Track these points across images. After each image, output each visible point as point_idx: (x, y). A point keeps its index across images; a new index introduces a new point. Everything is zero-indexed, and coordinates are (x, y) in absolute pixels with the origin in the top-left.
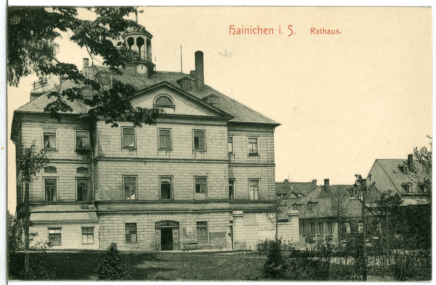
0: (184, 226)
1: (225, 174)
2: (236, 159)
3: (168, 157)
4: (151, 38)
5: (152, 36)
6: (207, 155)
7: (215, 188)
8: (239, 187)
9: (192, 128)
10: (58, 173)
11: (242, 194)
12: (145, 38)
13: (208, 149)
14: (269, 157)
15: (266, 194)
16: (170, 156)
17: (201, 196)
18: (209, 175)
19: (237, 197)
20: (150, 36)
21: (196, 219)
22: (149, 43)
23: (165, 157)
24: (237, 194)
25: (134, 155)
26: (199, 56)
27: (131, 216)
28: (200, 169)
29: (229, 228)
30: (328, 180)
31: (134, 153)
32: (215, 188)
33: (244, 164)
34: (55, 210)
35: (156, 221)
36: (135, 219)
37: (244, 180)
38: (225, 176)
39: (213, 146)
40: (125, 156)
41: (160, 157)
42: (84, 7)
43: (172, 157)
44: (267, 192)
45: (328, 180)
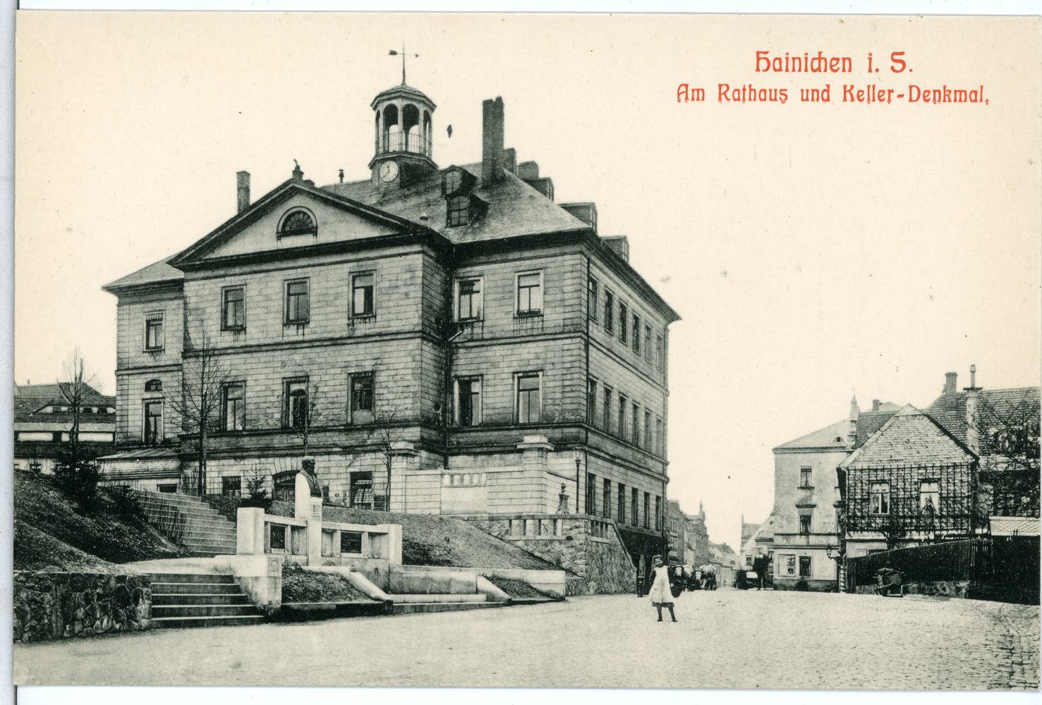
0: (326, 483)
1: (414, 363)
2: (485, 330)
3: (301, 338)
4: (433, 110)
5: (435, 106)
6: (377, 324)
7: (391, 396)
8: (490, 395)
9: (282, 278)
10: (165, 390)
11: (497, 411)
12: (422, 109)
13: (379, 311)
14: (567, 316)
15: (557, 407)
16: (304, 335)
17: (362, 416)
18: (382, 367)
19: (484, 417)
20: (432, 107)
21: (349, 466)
22: (428, 119)
23: (296, 338)
24: (485, 412)
25: (242, 340)
26: (295, 160)
27: (232, 462)
28: (360, 357)
29: (776, 576)
30: (955, 375)
31: (242, 337)
32: (391, 396)
33: (504, 338)
34: (41, 429)
35: (274, 473)
36: (239, 468)
37: (504, 376)
38: (412, 368)
39: (391, 304)
40: (226, 345)
41: (286, 339)
42: (404, 71)
43: (307, 338)
44: (558, 402)
45: (955, 375)
